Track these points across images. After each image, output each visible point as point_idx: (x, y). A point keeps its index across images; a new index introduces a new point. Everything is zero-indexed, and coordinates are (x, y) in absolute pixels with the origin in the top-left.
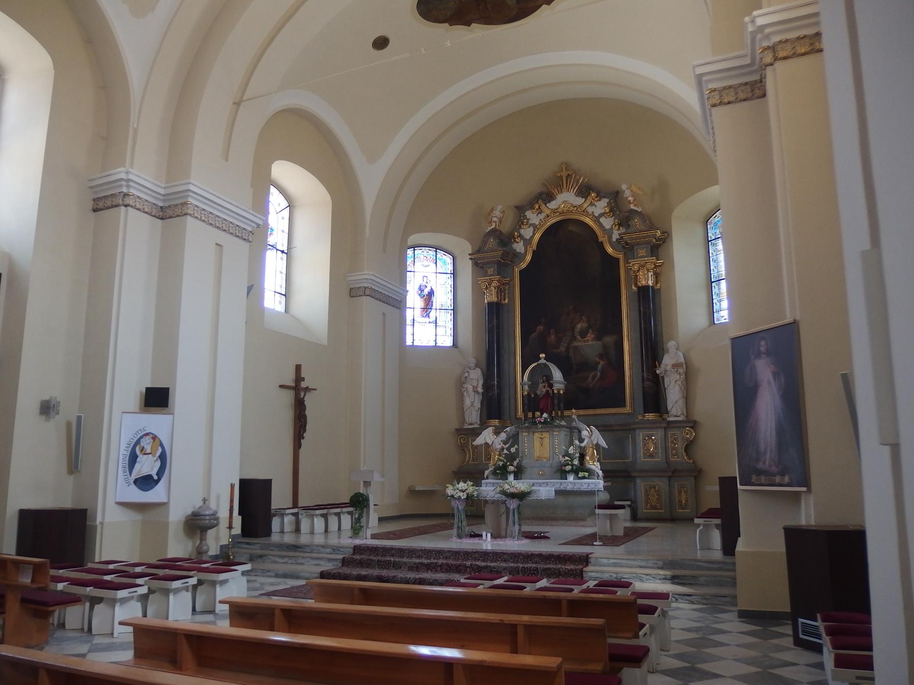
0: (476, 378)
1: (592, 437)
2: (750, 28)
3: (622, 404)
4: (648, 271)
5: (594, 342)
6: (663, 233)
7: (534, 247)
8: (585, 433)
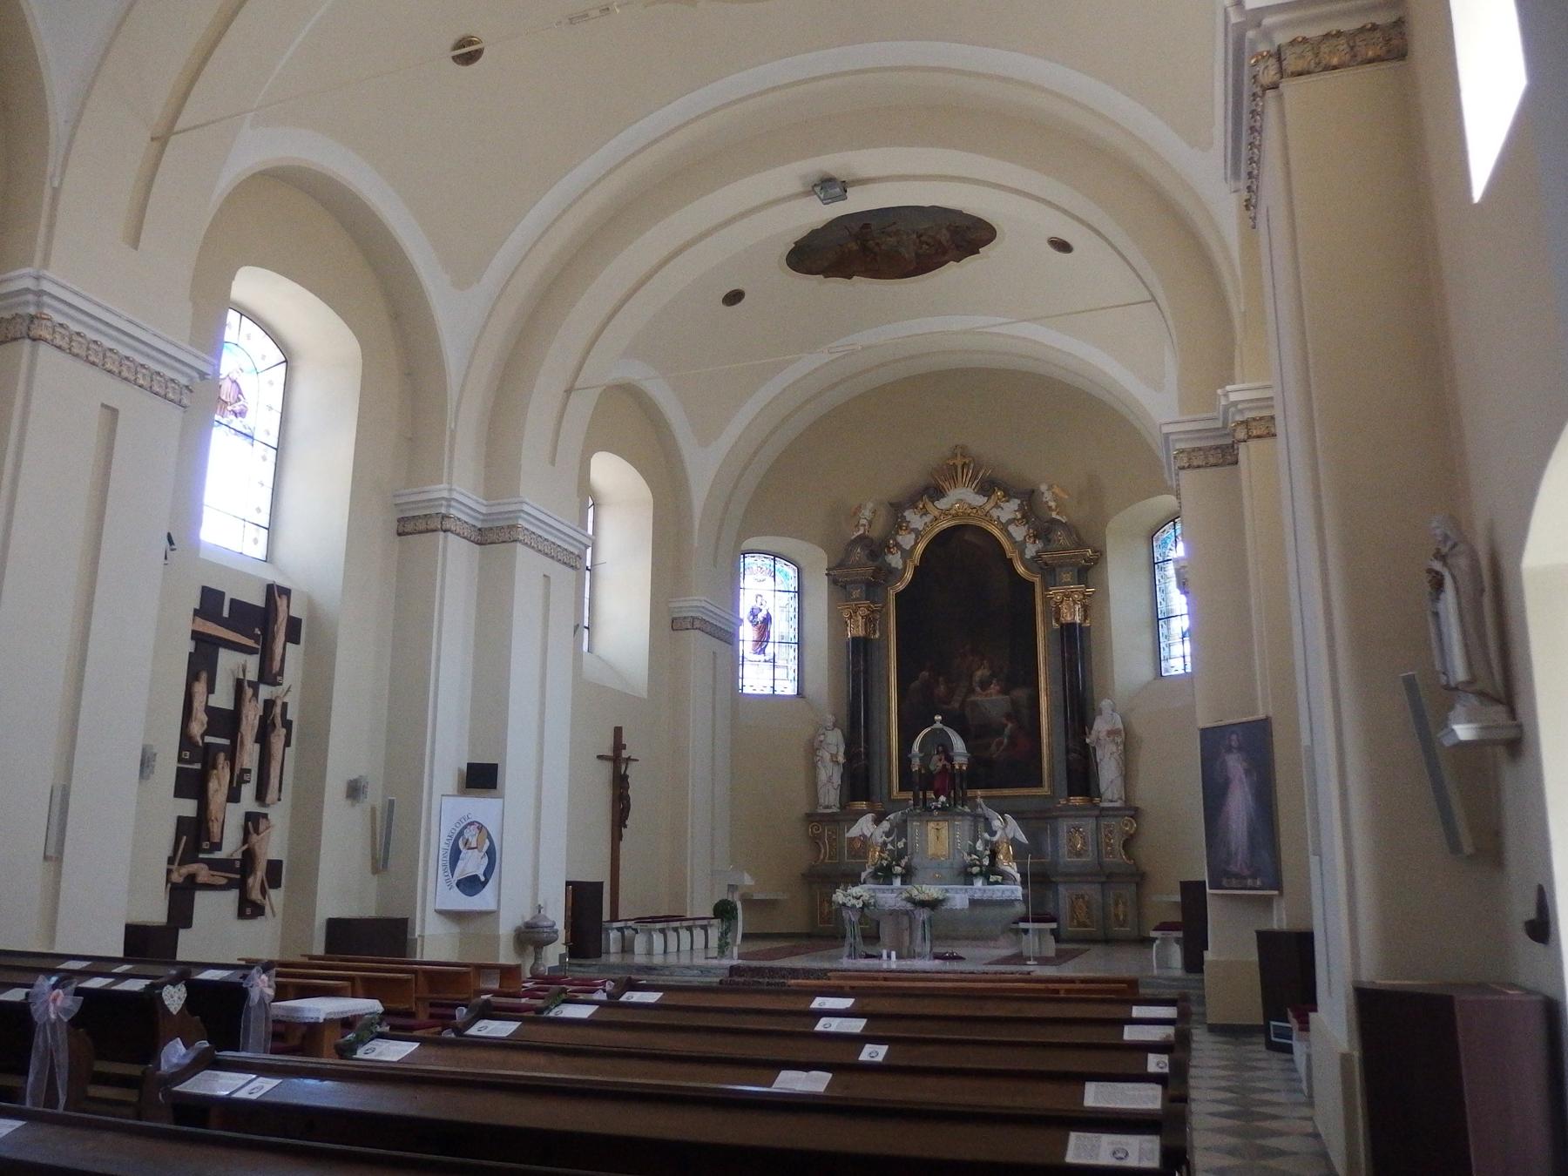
0: (835, 741)
1: (1007, 829)
2: (1223, 402)
3: (1038, 783)
4: (1075, 602)
5: (1001, 697)
6: (1095, 552)
7: (917, 562)
8: (997, 823)
